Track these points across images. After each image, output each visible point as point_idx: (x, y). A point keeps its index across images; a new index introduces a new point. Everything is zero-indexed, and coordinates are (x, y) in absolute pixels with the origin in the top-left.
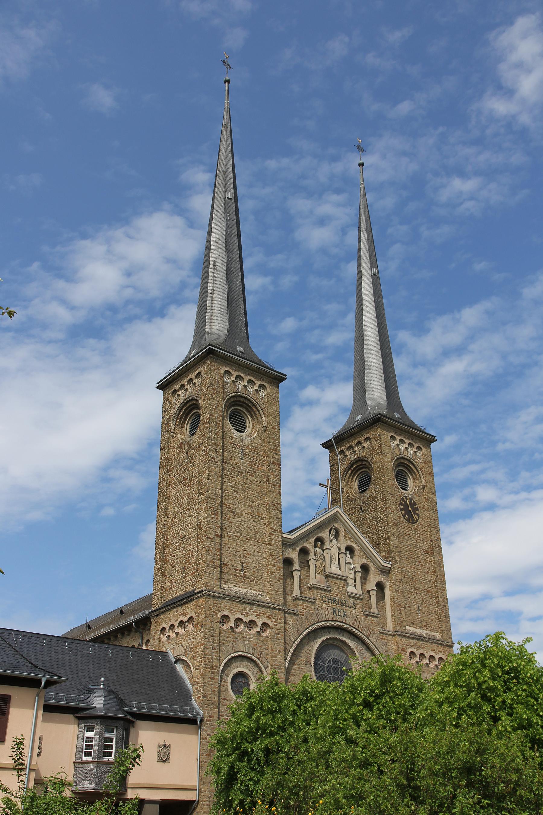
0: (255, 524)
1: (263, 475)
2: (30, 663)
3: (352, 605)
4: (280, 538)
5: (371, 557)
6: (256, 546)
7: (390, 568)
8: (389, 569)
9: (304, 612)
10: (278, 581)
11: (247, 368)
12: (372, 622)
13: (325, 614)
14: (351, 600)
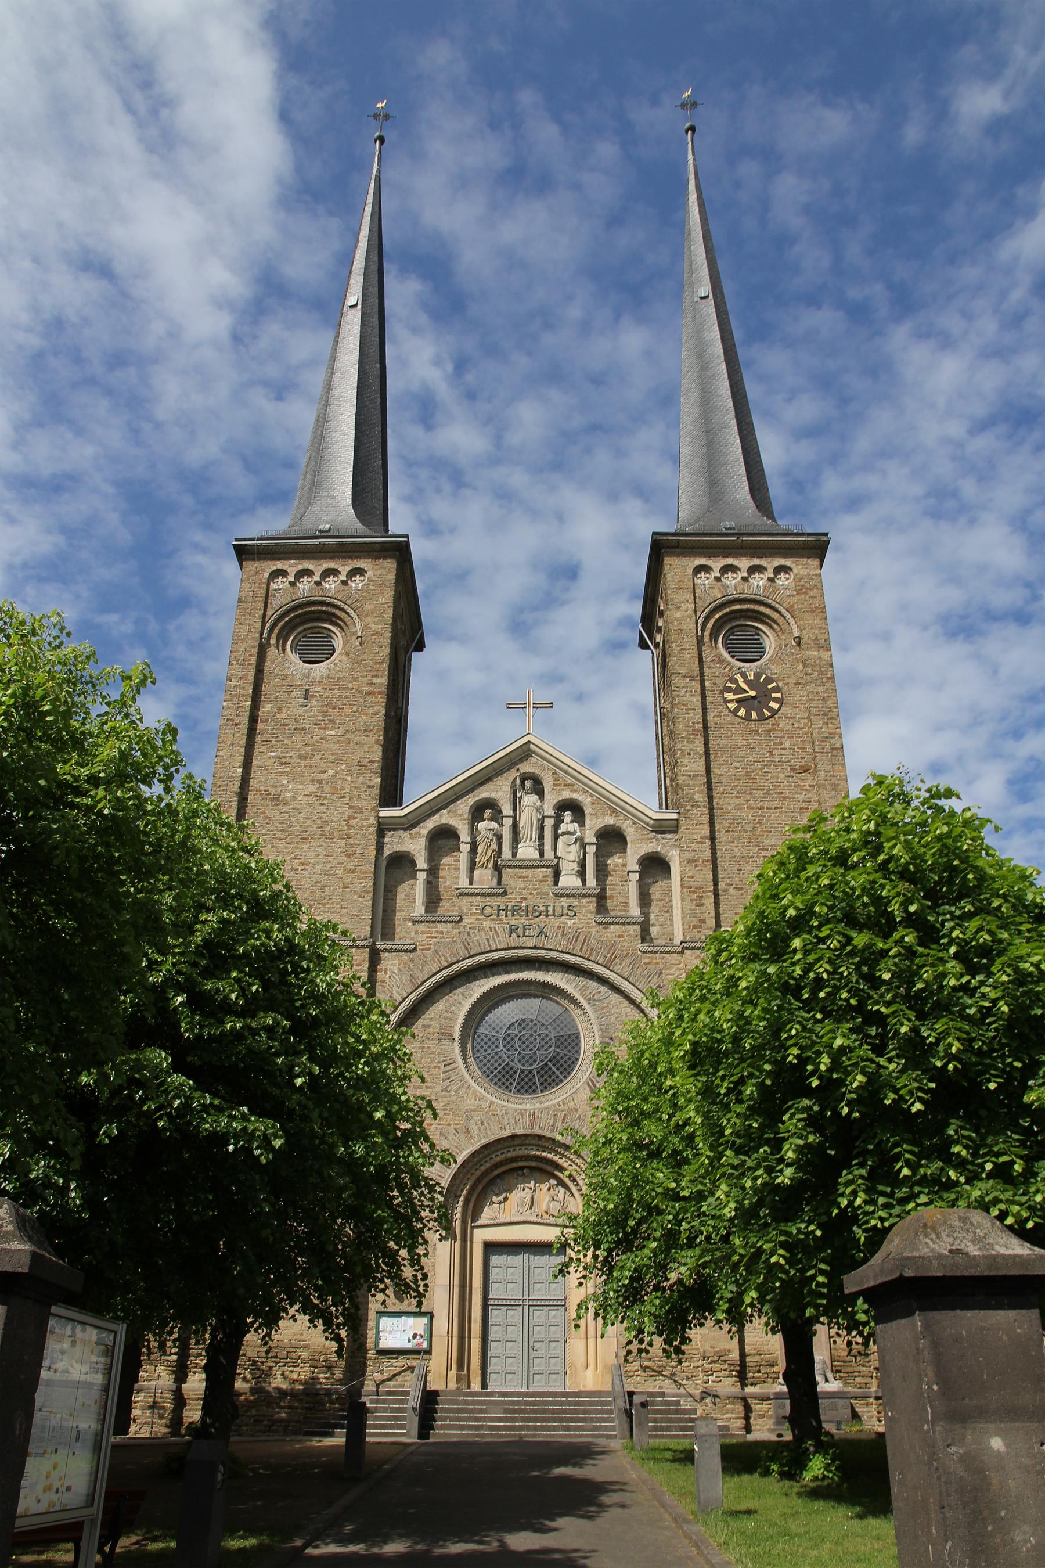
3: (565, 911)
4: (372, 820)
5: (623, 809)
7: (677, 820)
10: (360, 896)
11: (320, 552)
12: (620, 936)
13: (488, 940)
14: (565, 902)
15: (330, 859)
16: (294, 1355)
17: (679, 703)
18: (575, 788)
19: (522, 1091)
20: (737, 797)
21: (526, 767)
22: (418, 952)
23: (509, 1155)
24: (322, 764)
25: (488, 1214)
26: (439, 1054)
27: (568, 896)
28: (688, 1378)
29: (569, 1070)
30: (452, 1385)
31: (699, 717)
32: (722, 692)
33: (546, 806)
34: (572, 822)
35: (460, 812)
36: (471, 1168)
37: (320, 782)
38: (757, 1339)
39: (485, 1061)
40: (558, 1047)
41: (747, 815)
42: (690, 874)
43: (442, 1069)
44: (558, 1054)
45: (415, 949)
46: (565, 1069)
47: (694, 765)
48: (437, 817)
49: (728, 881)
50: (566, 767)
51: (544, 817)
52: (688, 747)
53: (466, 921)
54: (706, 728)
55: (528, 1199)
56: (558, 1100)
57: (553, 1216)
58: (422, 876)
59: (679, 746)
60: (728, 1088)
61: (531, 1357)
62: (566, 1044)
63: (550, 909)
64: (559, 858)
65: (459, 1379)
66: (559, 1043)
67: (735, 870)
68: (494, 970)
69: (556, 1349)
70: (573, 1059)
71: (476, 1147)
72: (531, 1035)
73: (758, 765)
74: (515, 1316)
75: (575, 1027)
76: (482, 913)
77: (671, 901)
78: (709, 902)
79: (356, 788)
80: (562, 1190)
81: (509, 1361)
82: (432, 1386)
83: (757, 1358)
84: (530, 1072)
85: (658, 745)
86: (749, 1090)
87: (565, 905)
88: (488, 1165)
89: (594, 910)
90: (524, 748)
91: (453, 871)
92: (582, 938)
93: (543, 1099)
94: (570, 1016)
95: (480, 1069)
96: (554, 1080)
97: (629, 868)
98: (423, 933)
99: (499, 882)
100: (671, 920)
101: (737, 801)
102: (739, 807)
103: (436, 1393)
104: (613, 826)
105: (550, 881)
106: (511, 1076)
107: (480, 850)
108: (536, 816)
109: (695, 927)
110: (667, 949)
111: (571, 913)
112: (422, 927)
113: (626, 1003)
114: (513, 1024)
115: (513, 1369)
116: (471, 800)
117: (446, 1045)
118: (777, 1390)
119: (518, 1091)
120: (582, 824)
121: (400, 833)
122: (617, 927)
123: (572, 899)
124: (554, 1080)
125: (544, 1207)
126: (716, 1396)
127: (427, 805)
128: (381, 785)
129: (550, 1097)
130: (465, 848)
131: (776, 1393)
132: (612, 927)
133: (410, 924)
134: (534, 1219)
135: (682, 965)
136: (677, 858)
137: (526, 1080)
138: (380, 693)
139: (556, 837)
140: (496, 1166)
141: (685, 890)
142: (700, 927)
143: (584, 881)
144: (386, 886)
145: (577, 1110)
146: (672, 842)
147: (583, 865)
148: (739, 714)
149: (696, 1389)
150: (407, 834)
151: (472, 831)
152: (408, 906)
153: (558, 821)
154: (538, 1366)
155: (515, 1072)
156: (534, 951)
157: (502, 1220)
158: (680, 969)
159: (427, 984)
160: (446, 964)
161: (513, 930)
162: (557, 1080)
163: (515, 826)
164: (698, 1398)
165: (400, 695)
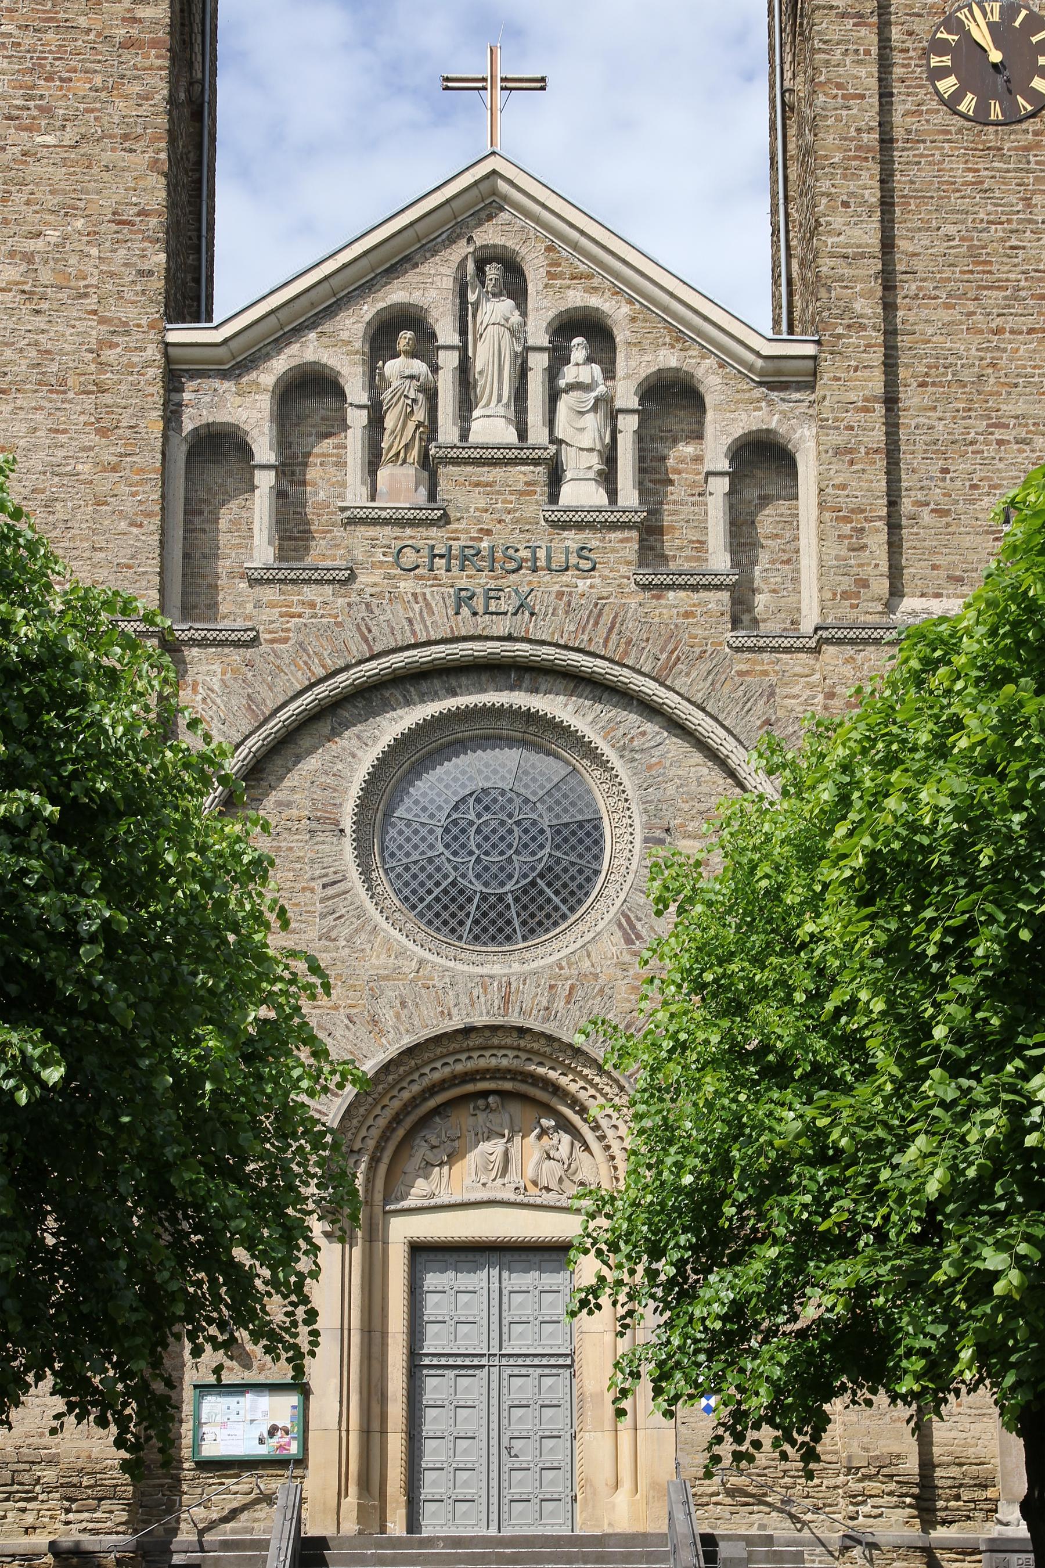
0: (40, 321)
1: (92, 111)
2: (732, 774)
3: (573, 560)
4: (152, 352)
5: (699, 333)
6: (42, 408)
7: (814, 358)
8: (810, 363)
9: (288, 630)
10: (132, 524)
12: (687, 615)
13: (410, 621)
14: (572, 539)
15: (62, 438)
16: (26, 1478)
17: (829, 80)
18: (596, 282)
19: (484, 937)
20: (947, 306)
21: (488, 235)
22: (264, 648)
23: (459, 1068)
24: (32, 218)
25: (420, 1190)
26: (312, 861)
27: (579, 526)
28: (817, 1509)
29: (580, 894)
30: (350, 1526)
31: (870, 117)
32: (925, 54)
33: (530, 328)
34: (589, 360)
35: (344, 335)
36: (383, 1095)
37: (28, 258)
38: (954, 1434)
39: (407, 876)
40: (558, 847)
41: (968, 347)
42: (837, 481)
43: (320, 892)
44: (558, 861)
45: (254, 642)
46: (572, 893)
47: (857, 232)
48: (294, 349)
49: (920, 496)
50: (575, 235)
51: (527, 349)
52: (844, 188)
53: (363, 579)
54: (886, 142)
55: (498, 1157)
56: (557, 956)
57: (548, 1189)
58: (265, 480)
59: (824, 185)
60: (941, 945)
61: (505, 1469)
62: (573, 840)
63: (541, 554)
64: (560, 442)
65: (363, 1512)
66: (558, 840)
67: (935, 471)
68: (424, 686)
69: (556, 1452)
70: (588, 872)
71: (392, 1052)
72: (502, 823)
73: (997, 231)
74: (472, 1388)
75: (592, 804)
76: (397, 563)
77: (796, 538)
78: (877, 540)
79: (112, 275)
80: (566, 1138)
81: (462, 1476)
82: (311, 1530)
83: (954, 1471)
84: (501, 898)
85: (774, 182)
86: (982, 948)
87: (574, 546)
88: (416, 1088)
89: (633, 557)
90: (484, 187)
91: (332, 470)
92: (607, 619)
93: (527, 955)
94: (582, 782)
95: (398, 892)
96: (548, 916)
97: (709, 466)
98: (272, 605)
99: (432, 496)
100: (796, 580)
101: (946, 316)
102: (949, 329)
103: (321, 1543)
104: (677, 370)
105: (541, 493)
106: (461, 908)
107: (389, 422)
108: (509, 346)
109: (846, 595)
110: (786, 643)
111: (586, 565)
112: (269, 593)
113: (698, 757)
114: (463, 800)
115: (469, 1492)
116: (368, 310)
117: (326, 844)
118: (994, 1535)
119: (476, 938)
120: (610, 374)
121: (216, 383)
122: (682, 594)
123: (587, 534)
124: (548, 916)
125: (530, 1173)
126: (873, 1546)
127: (272, 320)
128: (168, 270)
129: (540, 950)
130: (357, 419)
131: (992, 1540)
132: (671, 594)
133: (243, 585)
134: (510, 1195)
135: (817, 676)
136: (812, 444)
137: (492, 915)
138: (154, 44)
139: (553, 397)
140: (432, 1090)
141: (827, 515)
142: (857, 595)
143: (612, 494)
144: (187, 501)
145: (596, 976)
146: (802, 408)
147: (610, 458)
148: (962, 108)
149: (831, 1530)
150: (227, 385)
151: (372, 378)
152: (239, 546)
153: (559, 358)
154: (520, 1485)
155: (470, 900)
156: (508, 645)
157: (444, 1199)
158: (812, 686)
159: (283, 715)
160: (321, 672)
161: (462, 600)
162: (556, 916)
163: (465, 368)
164: (835, 1548)
165: (197, 48)
